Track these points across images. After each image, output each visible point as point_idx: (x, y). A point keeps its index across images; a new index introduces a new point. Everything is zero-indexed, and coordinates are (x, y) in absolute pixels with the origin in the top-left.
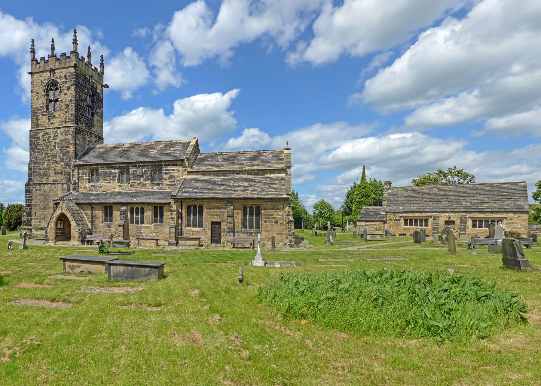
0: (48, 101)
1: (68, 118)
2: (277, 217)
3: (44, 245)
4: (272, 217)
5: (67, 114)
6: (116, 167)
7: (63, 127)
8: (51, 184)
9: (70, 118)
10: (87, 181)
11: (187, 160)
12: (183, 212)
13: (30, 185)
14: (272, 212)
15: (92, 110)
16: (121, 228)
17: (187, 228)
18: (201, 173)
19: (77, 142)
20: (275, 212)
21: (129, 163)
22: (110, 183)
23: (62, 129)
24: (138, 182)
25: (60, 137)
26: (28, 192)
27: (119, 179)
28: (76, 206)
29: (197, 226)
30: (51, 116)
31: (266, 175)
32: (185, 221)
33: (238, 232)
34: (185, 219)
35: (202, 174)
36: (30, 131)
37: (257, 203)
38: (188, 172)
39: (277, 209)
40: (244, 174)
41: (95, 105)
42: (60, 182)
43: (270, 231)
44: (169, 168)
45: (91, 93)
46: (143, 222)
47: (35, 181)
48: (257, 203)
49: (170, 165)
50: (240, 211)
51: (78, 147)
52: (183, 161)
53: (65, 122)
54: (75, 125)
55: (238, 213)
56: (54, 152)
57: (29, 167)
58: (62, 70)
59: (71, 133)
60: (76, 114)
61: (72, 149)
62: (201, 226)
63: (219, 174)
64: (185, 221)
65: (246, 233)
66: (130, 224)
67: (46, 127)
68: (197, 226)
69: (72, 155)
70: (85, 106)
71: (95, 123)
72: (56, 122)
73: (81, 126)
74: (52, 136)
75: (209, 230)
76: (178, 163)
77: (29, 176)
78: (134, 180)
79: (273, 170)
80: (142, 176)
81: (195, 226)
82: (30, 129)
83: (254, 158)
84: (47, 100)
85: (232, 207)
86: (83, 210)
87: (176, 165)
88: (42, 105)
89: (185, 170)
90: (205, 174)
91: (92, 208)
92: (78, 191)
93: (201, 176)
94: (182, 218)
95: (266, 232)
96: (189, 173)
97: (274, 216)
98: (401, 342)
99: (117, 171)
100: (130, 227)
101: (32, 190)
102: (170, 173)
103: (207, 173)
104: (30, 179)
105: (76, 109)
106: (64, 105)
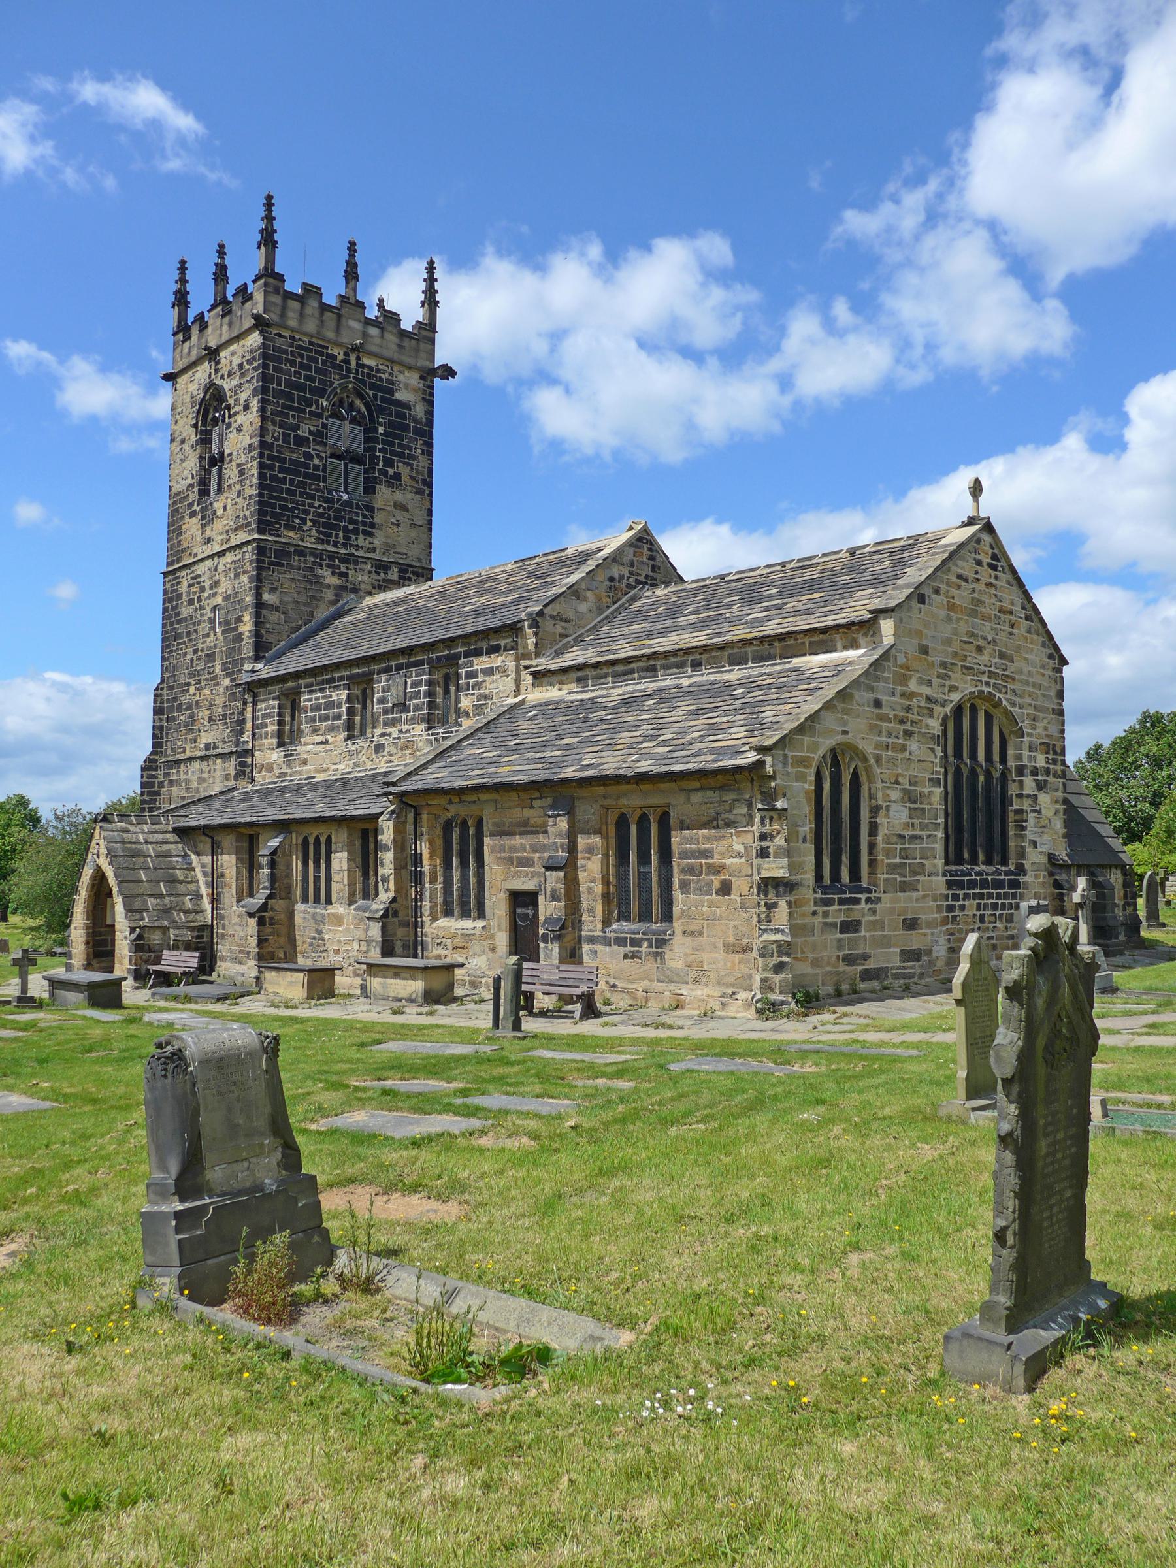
0: (206, 464)
1: (242, 514)
2: (728, 862)
3: (399, 1019)
4: (709, 865)
5: (239, 500)
6: (341, 679)
7: (230, 549)
8: (202, 758)
9: (247, 513)
10: (275, 741)
11: (530, 627)
12: (424, 848)
13: (156, 769)
14: (708, 839)
15: (366, 471)
16: (253, 922)
17: (443, 922)
18: (575, 675)
19: (266, 597)
20: (718, 839)
21: (373, 659)
22: (325, 742)
23: (229, 558)
24: (394, 731)
25: (225, 587)
26: (149, 793)
27: (350, 726)
28: (177, 839)
29: (456, 910)
30: (207, 517)
31: (796, 662)
32: (432, 892)
33: (592, 940)
34: (433, 881)
35: (579, 680)
36: (165, 574)
37: (653, 799)
38: (535, 675)
39: (728, 825)
40: (716, 664)
41: (380, 450)
42: (220, 751)
43: (701, 934)
44: (478, 664)
45: (363, 410)
46: (329, 901)
47: (169, 752)
48: (653, 799)
49: (478, 653)
50: (596, 840)
51: (273, 617)
52: (514, 629)
53: (236, 529)
54: (256, 536)
55: (590, 850)
56: (210, 641)
57: (155, 701)
58: (234, 347)
59: (247, 567)
60: (260, 495)
61: (247, 627)
62: (481, 914)
63: (632, 672)
64: (432, 892)
65: (620, 942)
66: (299, 907)
67: (196, 555)
68: (456, 910)
69: (248, 650)
70: (316, 461)
71: (378, 518)
72: (217, 529)
73: (289, 536)
74: (207, 585)
75: (500, 930)
76: (502, 643)
77: (154, 736)
78: (385, 724)
79: (823, 631)
80: (404, 708)
81: (465, 914)
82: (165, 569)
83: (790, 591)
84: (201, 458)
85: (563, 824)
86: (198, 854)
87: (495, 650)
88: (190, 481)
89: (526, 668)
90: (586, 678)
91: (213, 843)
92: (253, 780)
93: (574, 687)
94: (418, 878)
95: (689, 939)
96: (540, 677)
97: (716, 860)
98: (246, 1546)
99: (344, 694)
100: (298, 920)
101: (161, 784)
102: (478, 685)
103: (593, 672)
104: (157, 745)
105: (261, 476)
106: (234, 467)
